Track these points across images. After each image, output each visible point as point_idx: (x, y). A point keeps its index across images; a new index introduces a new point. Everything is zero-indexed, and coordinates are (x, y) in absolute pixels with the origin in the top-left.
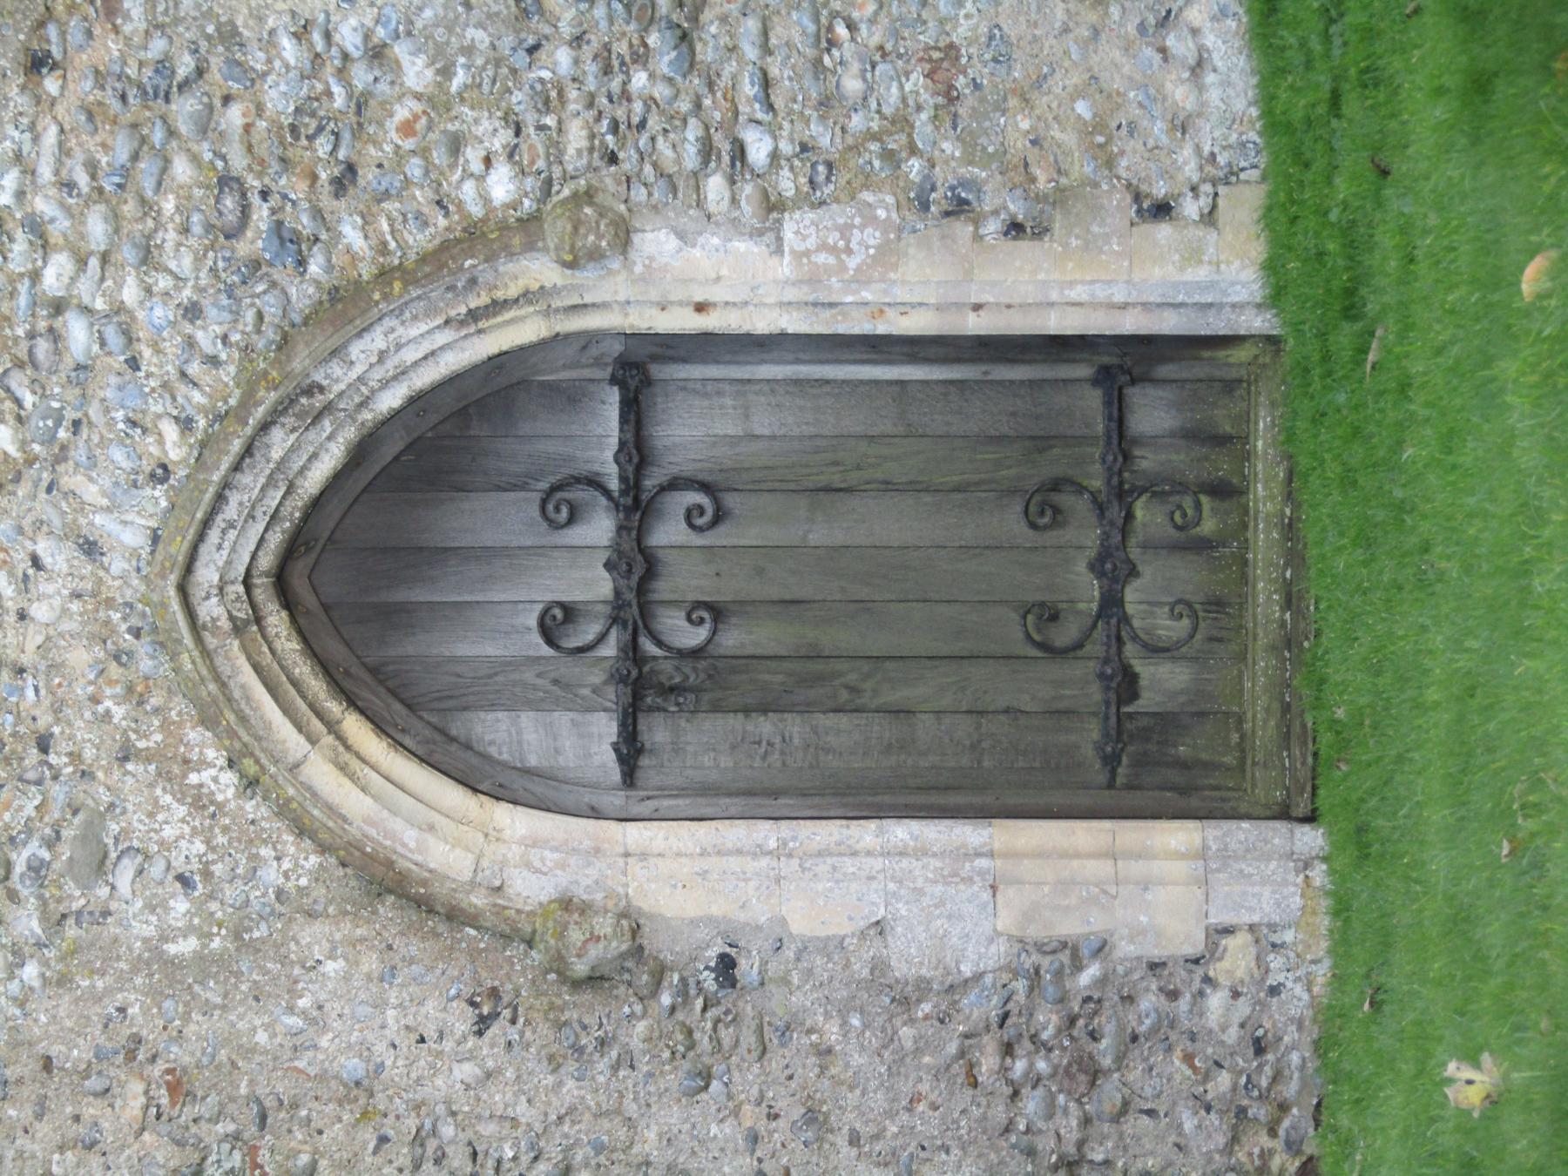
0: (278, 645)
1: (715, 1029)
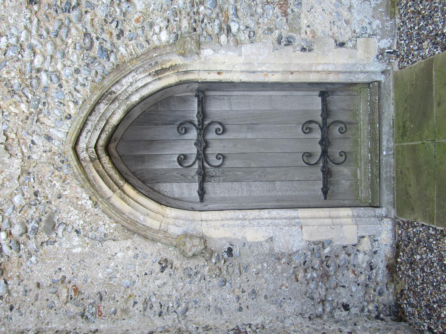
0: (105, 166)
1: (227, 268)
